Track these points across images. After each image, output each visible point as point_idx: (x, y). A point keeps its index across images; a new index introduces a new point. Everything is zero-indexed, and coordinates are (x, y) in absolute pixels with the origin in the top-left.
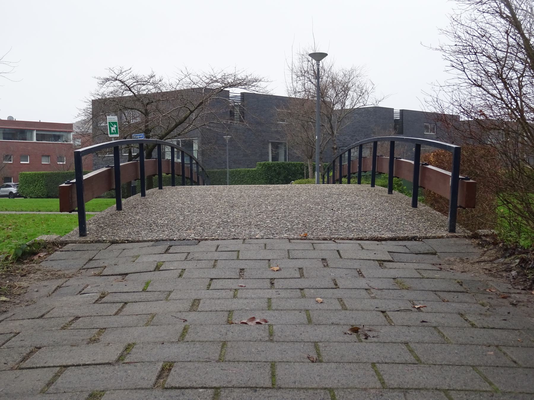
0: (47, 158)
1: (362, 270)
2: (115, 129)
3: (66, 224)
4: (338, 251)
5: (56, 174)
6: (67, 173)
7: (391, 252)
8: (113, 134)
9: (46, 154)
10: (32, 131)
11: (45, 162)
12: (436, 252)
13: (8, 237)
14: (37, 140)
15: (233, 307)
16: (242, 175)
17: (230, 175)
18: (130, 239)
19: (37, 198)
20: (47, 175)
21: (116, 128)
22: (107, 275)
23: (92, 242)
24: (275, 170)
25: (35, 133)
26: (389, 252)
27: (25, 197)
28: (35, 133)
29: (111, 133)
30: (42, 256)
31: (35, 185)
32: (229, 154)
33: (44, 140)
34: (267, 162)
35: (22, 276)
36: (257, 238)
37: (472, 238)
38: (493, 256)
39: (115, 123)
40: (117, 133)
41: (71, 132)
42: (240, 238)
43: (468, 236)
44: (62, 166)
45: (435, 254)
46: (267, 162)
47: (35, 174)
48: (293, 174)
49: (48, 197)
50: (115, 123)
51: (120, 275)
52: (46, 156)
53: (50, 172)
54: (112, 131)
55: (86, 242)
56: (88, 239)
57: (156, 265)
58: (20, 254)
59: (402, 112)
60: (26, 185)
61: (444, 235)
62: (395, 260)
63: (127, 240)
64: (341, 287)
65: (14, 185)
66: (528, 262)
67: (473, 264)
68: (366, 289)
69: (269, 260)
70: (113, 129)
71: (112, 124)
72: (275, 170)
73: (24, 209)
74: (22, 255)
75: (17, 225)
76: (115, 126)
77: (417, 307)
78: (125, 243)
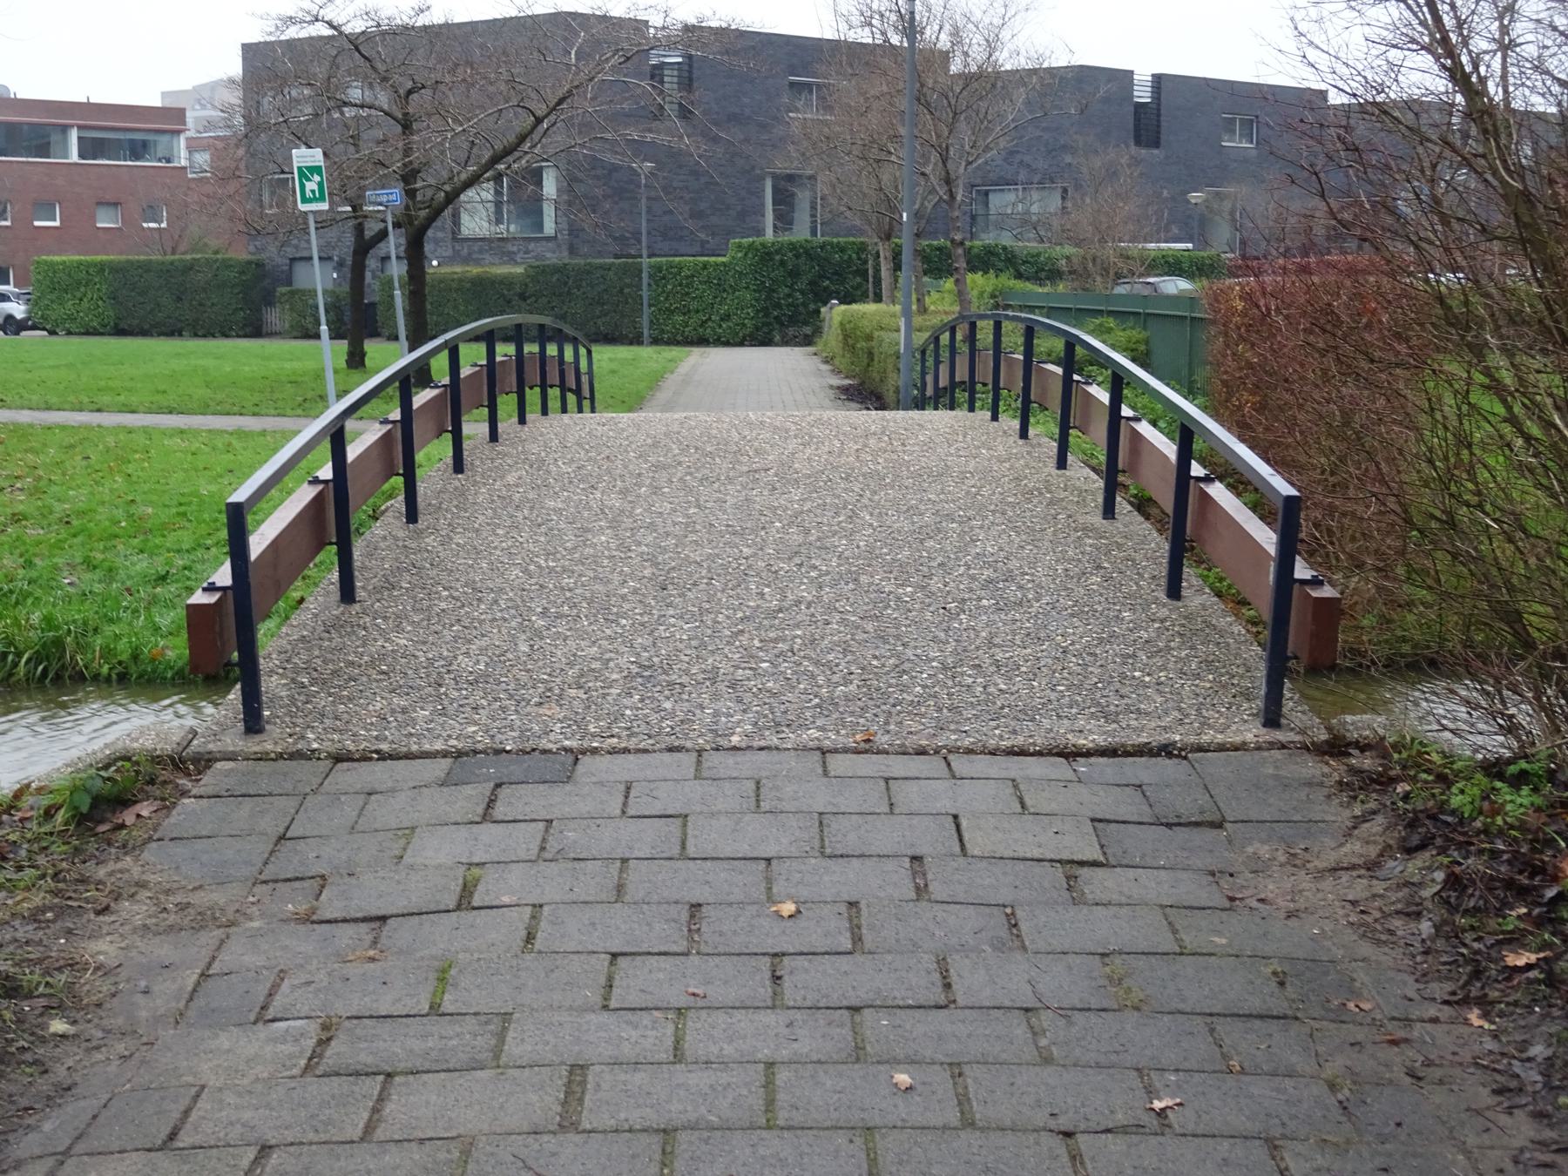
0: (110, 211)
1: (1020, 913)
2: (316, 187)
3: (180, 475)
4: (956, 817)
5: (146, 267)
6: (172, 263)
7: (1100, 821)
8: (310, 201)
9: (109, 197)
10: (65, 129)
11: (106, 221)
12: (1224, 820)
13: (17, 518)
14: (81, 156)
15: (677, 1110)
16: (687, 277)
17: (650, 276)
18: (384, 747)
19: (87, 333)
20: (116, 269)
21: (320, 184)
22: (329, 922)
23: (280, 756)
24: (782, 263)
25: (74, 135)
26: (1093, 820)
27: (52, 333)
28: (74, 135)
29: (305, 200)
30: (145, 813)
31: (79, 295)
32: (649, 211)
33: (103, 157)
34: (761, 239)
35: (98, 913)
36: (735, 748)
37: (1325, 753)
38: (1375, 842)
39: (315, 170)
40: (322, 199)
41: (179, 132)
42: (689, 744)
43: (1313, 743)
44: (157, 236)
45: (1218, 825)
46: (758, 240)
47: (80, 263)
48: (836, 273)
49: (120, 332)
50: (317, 170)
51: (365, 920)
52: (108, 204)
53: (123, 258)
54: (309, 194)
55: (262, 758)
56: (269, 746)
57: (461, 881)
58: (85, 805)
59: (1159, 80)
60: (53, 296)
61: (1249, 737)
62: (1113, 861)
63: (377, 752)
64: (961, 1001)
65: (18, 296)
66: (1466, 887)
67: (1320, 874)
68: (1027, 1010)
69: (768, 860)
70: (311, 186)
71: (307, 172)
72: (782, 263)
73: (54, 400)
74: (93, 806)
75: (40, 478)
76: (317, 178)
77: (1158, 1105)
78: (371, 759)
